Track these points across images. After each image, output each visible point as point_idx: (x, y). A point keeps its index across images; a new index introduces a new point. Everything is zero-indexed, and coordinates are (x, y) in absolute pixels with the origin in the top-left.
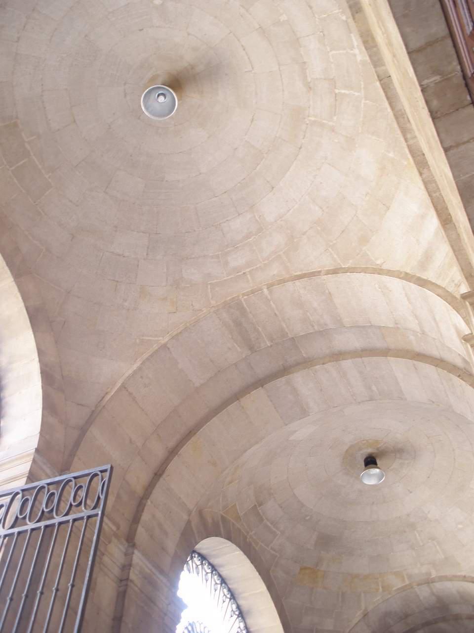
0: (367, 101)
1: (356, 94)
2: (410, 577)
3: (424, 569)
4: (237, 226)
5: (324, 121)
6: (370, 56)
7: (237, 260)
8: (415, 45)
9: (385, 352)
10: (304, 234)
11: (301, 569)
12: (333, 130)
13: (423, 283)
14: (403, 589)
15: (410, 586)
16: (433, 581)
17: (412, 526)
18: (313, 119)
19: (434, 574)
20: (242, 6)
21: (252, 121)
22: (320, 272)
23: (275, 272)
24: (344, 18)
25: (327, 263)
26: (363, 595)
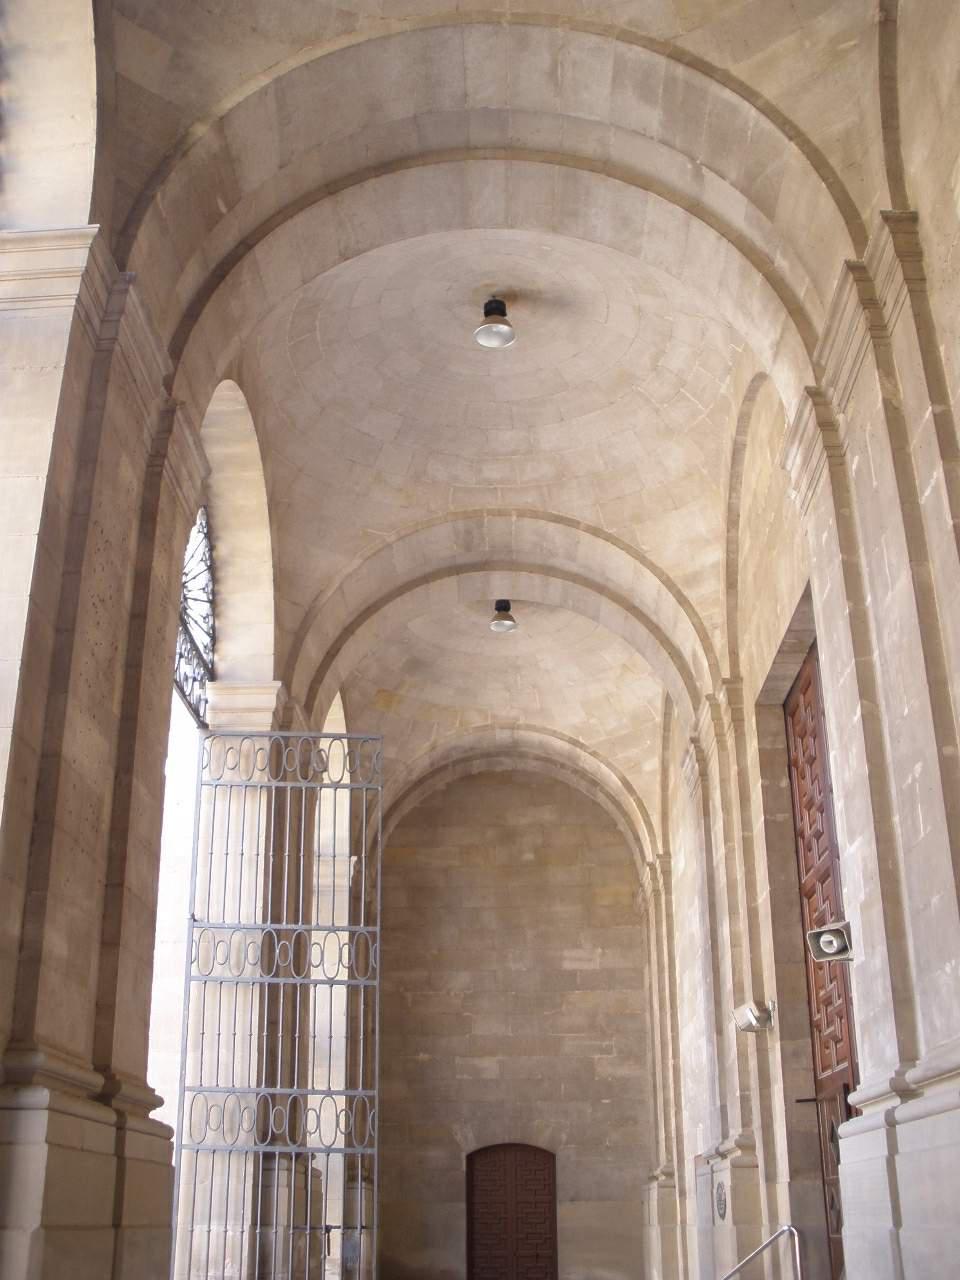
1: (700, 406)
2: (494, 717)
3: (514, 713)
4: (508, 438)
7: (492, 472)
8: (792, 628)
9: (601, 589)
10: (577, 477)
11: (379, 692)
12: (657, 411)
13: (682, 601)
14: (485, 728)
15: (492, 727)
16: (519, 727)
17: (517, 668)
18: (642, 390)
19: (521, 722)
21: (575, 356)
22: (579, 523)
23: (530, 500)
25: (588, 516)
26: (436, 726)
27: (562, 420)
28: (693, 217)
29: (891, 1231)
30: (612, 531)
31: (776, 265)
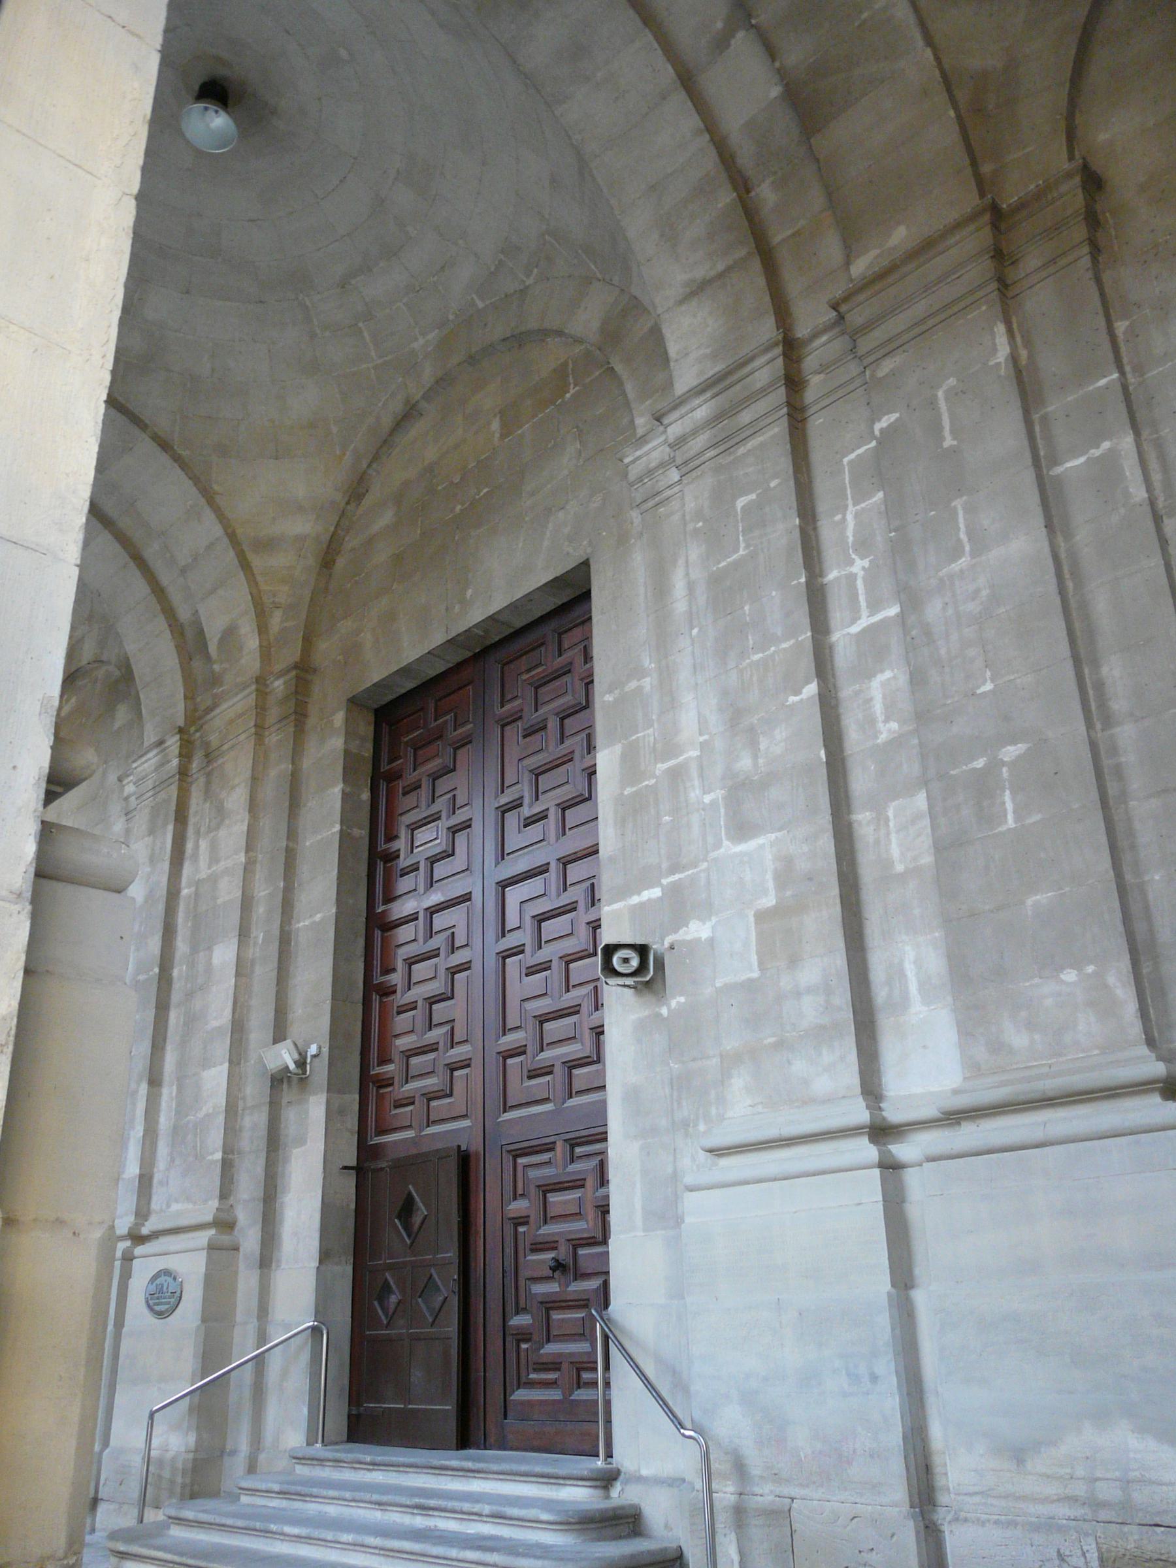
0: (373, 371)
1: (373, 353)
5: (315, 320)
6: (430, 388)
18: (308, 303)
20: (398, 172)
24: (451, 317)
27: (187, 292)
28: (682, 89)
29: (889, 1294)
30: (184, 453)
31: (753, 194)
